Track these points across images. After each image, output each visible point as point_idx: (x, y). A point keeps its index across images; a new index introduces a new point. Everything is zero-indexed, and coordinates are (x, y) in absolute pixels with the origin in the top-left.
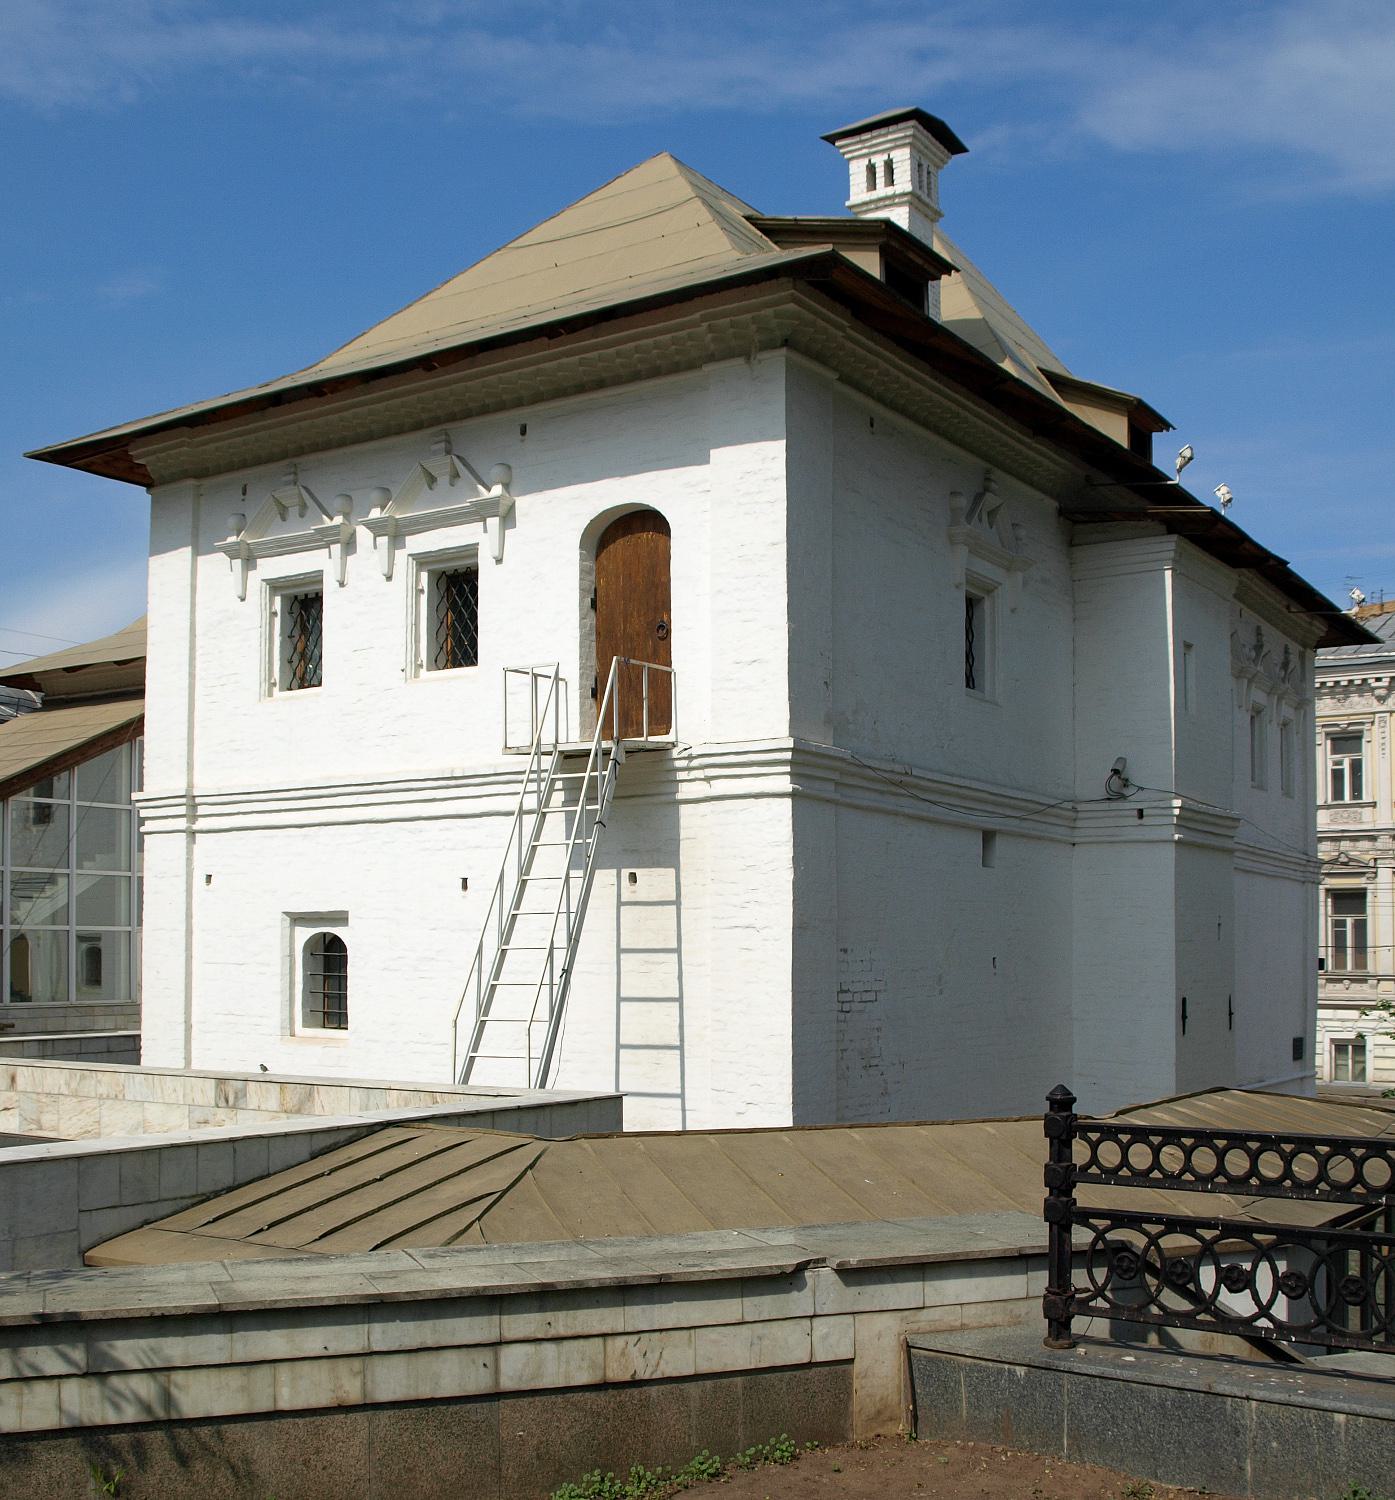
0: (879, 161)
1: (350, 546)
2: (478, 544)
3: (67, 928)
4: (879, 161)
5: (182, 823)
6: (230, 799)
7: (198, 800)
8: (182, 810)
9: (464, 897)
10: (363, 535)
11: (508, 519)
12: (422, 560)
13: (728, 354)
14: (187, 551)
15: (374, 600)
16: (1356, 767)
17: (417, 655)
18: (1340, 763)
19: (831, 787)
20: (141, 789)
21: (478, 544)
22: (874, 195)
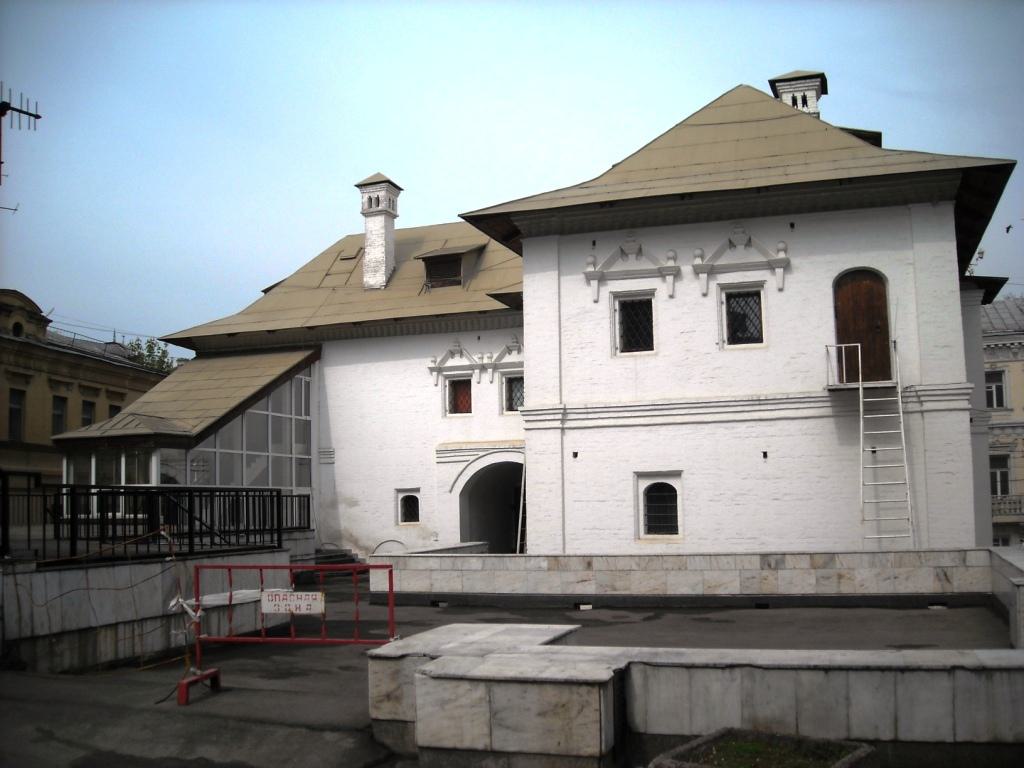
0: (799, 96)
1: (677, 274)
2: (655, 289)
3: (240, 452)
4: (799, 96)
5: (558, 424)
6: (588, 411)
7: (568, 411)
8: (560, 416)
9: (769, 447)
10: (687, 269)
11: (786, 266)
12: (723, 287)
13: (555, 233)
14: (555, 274)
15: (687, 310)
16: (1000, 390)
17: (615, 344)
18: (990, 387)
19: (966, 402)
20: (522, 404)
21: (655, 289)
22: (371, 210)
